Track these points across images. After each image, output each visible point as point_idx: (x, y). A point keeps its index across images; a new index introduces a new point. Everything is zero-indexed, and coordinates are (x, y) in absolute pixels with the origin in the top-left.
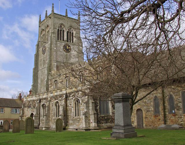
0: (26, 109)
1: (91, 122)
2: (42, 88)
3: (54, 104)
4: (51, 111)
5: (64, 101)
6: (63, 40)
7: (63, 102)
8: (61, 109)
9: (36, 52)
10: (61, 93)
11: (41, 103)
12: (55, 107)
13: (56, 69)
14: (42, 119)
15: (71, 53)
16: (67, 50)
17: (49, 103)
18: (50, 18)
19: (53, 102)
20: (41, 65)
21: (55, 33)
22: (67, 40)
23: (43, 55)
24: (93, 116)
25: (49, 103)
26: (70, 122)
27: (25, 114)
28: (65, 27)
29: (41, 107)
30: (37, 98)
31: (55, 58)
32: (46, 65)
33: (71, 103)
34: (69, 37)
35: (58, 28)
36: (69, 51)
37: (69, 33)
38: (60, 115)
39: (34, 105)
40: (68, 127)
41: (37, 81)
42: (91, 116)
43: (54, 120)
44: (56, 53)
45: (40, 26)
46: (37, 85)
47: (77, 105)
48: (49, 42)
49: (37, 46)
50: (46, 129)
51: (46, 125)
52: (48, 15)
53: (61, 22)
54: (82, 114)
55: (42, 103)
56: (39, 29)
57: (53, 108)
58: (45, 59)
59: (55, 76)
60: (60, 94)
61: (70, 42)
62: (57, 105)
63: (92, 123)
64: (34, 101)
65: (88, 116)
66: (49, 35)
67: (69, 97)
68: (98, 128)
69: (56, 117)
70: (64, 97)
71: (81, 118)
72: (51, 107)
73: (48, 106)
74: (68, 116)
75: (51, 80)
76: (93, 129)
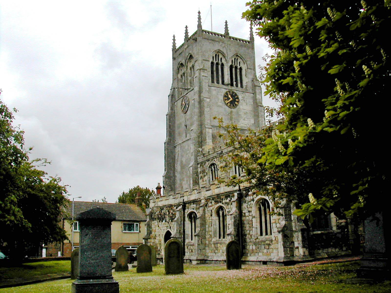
0: (155, 224)
2: (185, 182)
3: (213, 211)
4: (207, 226)
5: (234, 204)
6: (223, 83)
7: (233, 209)
8: (230, 221)
9: (170, 108)
11: (186, 211)
12: (217, 218)
13: (211, 141)
14: (189, 242)
15: (239, 108)
16: (233, 101)
17: (204, 210)
19: (211, 208)
20: (179, 134)
21: (206, 70)
22: (230, 83)
23: (183, 115)
24: (300, 234)
25: (204, 210)
26: (250, 247)
27: (153, 233)
29: (187, 219)
30: (176, 201)
31: (208, 120)
32: (193, 135)
33: (251, 209)
34: (234, 77)
35: (211, 60)
36: (236, 105)
37: (234, 69)
38: (228, 235)
39: (171, 215)
40: (245, 258)
41: (174, 167)
42: (295, 235)
43: (214, 244)
44: (211, 109)
45: (174, 59)
46: (175, 176)
47: (263, 213)
48: (196, 89)
49: (170, 97)
50: (199, 262)
51: (198, 254)
53: (217, 47)
54: (275, 230)
55: (187, 211)
56: (173, 63)
57: (213, 220)
58: (188, 123)
59: (211, 156)
60: (226, 191)
61: (237, 86)
62: (221, 213)
63: (298, 248)
64: (171, 206)
65: (289, 235)
66: (194, 75)
67: (246, 197)
68: (311, 259)
69: (218, 238)
70: (236, 197)
71: (274, 239)
72: (208, 218)
73: (202, 215)
74: (246, 235)
75: (202, 164)
76: (300, 260)
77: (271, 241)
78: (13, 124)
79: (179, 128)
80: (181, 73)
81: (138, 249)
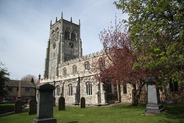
1: (102, 99)
2: (51, 73)
5: (77, 83)
10: (74, 77)
17: (63, 85)
18: (60, 22)
19: (66, 84)
20: (51, 56)
25: (63, 85)
28: (70, 30)
45: (51, 28)
52: (58, 20)
58: (55, 52)
63: (103, 100)
77: (92, 97)
78: (100, 51)
79: (51, 54)
80: (53, 34)
81: (16, 105)
